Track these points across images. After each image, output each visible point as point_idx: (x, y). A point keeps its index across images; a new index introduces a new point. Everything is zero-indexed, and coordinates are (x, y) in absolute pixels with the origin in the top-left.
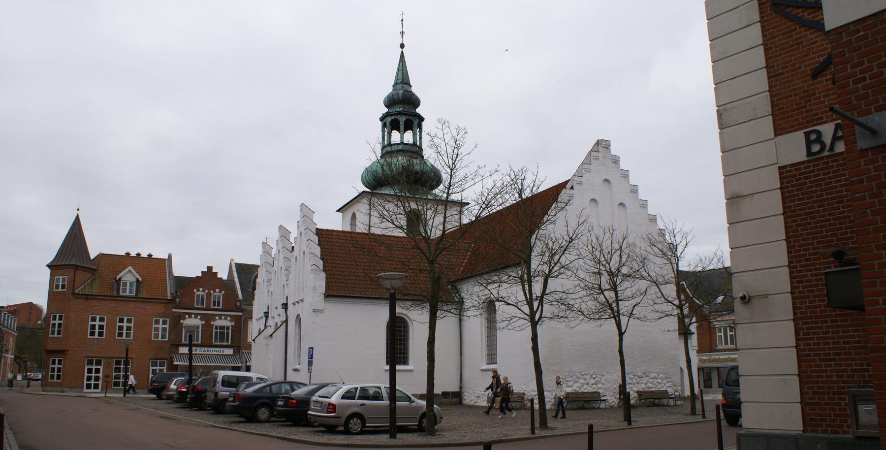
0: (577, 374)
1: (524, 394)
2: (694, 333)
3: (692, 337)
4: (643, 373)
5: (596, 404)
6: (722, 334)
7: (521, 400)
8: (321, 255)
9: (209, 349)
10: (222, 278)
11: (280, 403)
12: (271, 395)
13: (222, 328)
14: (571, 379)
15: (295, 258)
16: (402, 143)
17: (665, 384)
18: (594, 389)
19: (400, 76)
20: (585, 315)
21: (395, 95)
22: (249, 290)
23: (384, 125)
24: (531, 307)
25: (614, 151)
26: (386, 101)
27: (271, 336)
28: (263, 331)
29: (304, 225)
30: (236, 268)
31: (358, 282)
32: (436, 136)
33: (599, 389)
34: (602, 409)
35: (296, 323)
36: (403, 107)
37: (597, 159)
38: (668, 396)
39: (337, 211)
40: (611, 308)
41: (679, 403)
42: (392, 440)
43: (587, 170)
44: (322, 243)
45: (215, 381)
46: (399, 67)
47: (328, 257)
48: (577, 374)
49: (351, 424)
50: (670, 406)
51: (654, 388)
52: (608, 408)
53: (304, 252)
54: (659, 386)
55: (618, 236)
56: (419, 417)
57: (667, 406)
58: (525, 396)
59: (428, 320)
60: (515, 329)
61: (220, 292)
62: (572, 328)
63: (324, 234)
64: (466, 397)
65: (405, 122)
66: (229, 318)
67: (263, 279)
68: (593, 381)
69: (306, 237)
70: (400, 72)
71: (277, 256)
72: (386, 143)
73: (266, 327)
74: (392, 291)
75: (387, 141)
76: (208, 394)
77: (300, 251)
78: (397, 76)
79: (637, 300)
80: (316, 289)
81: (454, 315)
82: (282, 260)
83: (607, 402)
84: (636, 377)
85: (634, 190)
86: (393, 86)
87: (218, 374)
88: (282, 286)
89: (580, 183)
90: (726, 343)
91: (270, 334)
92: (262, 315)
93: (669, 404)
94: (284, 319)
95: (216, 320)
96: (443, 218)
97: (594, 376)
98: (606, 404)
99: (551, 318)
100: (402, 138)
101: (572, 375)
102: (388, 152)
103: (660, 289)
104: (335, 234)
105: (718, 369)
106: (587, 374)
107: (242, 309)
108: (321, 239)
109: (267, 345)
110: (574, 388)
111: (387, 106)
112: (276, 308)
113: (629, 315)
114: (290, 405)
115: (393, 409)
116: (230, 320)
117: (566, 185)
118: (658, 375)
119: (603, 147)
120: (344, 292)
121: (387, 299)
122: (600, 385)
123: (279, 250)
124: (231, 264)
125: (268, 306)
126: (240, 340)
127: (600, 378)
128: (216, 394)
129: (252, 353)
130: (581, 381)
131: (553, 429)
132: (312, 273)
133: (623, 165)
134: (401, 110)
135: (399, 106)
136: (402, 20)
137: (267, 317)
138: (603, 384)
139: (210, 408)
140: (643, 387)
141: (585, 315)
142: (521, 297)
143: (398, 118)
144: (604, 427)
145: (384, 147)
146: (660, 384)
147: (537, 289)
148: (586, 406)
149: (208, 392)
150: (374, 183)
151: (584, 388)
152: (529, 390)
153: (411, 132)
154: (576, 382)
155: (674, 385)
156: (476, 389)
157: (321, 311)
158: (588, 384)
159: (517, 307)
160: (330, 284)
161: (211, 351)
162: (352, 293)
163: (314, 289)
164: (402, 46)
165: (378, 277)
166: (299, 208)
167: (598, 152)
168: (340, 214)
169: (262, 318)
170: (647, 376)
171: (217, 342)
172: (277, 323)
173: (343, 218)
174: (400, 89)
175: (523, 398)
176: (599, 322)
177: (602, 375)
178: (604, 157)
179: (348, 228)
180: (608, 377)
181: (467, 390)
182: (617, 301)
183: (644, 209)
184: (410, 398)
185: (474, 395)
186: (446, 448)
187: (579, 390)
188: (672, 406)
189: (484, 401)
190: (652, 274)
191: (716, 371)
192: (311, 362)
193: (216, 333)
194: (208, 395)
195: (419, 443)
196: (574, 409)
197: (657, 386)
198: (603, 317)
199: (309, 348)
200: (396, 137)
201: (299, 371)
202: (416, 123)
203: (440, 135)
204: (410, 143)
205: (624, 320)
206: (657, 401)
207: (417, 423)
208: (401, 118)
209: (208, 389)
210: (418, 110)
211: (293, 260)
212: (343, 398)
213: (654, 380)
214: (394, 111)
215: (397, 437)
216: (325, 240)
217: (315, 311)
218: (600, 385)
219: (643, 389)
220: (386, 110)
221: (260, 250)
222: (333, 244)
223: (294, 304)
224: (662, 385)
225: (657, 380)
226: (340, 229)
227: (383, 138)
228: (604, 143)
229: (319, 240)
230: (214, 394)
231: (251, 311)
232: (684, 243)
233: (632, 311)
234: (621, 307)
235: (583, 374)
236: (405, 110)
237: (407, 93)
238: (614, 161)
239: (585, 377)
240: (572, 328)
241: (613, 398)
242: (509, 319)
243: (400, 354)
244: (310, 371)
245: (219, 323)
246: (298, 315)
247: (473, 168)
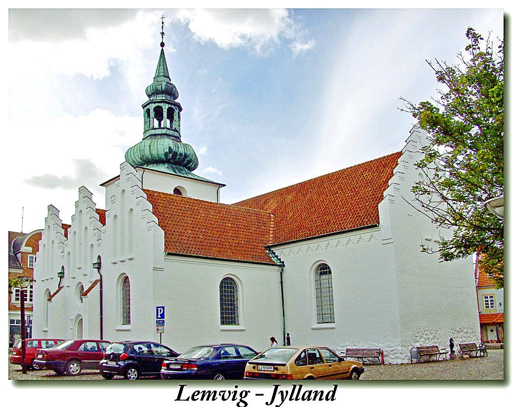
84: (456, 332)
111: (149, 96)
134: (163, 98)
138: (438, 339)
145: (145, 132)
158: (428, 339)
202: (177, 111)
217: (155, 269)
220: (147, 99)
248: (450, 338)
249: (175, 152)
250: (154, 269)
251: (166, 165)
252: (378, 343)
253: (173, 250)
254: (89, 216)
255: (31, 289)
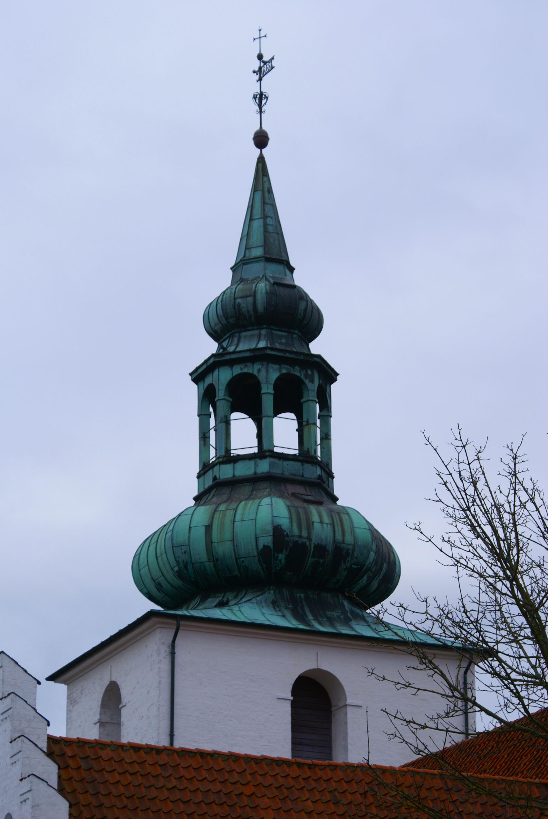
19: (257, 237)
36: (270, 337)
46: (251, 208)
65: (277, 385)
69: (18, 766)
70: (257, 224)
72: (213, 453)
78: (246, 236)
86: (234, 269)
111: (215, 335)
134: (262, 344)
135: (256, 332)
143: (255, 373)
150: (177, 582)
153: (292, 416)
173: (71, 701)
174: (257, 279)
202: (312, 387)
208: (263, 371)
227: (204, 437)
236: (278, 346)
249: (296, 543)
251: (270, 595)
253: (294, 269)
254: (17, 771)
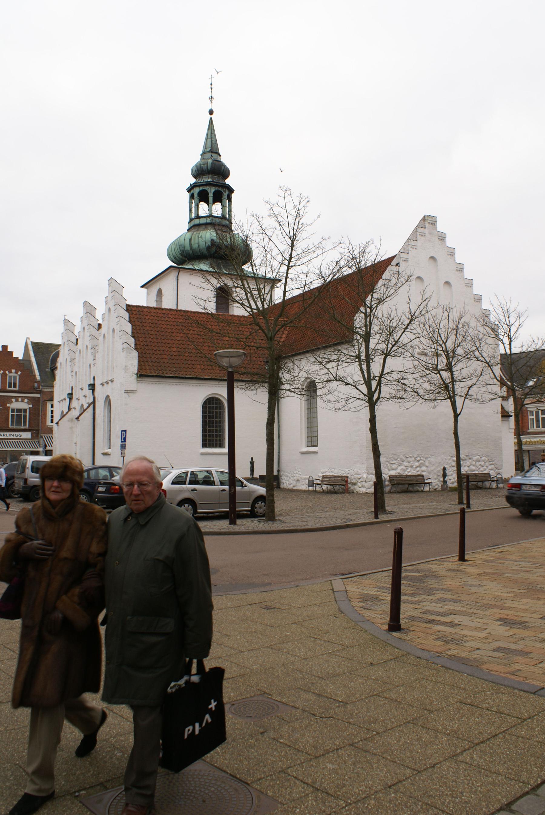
0: (401, 456)
1: (347, 477)
2: (511, 416)
3: (509, 420)
4: (467, 456)
5: (420, 487)
6: (534, 417)
7: (345, 484)
8: (132, 333)
9: (6, 433)
10: (18, 358)
11: (101, 489)
12: (90, 481)
13: (19, 410)
14: (395, 462)
15: (102, 335)
16: (210, 216)
17: (487, 467)
18: (418, 471)
19: (209, 145)
20: (420, 396)
21: (204, 164)
22: (47, 370)
23: (192, 197)
24: (369, 387)
25: (441, 227)
26: (194, 170)
27: (78, 418)
28: (67, 413)
29: (113, 301)
30: (33, 347)
31: (171, 361)
32: (277, 203)
33: (423, 471)
34: (426, 492)
35: (104, 404)
36: (212, 178)
37: (423, 235)
38: (491, 478)
39: (142, 287)
40: (446, 387)
41: (501, 485)
42: (233, 527)
43: (413, 247)
44: (133, 320)
45: (24, 468)
46: (207, 135)
47: (139, 335)
48: (401, 456)
49: (256, 508)
50: (492, 489)
51: (477, 470)
52: (432, 491)
53: (114, 330)
54: (482, 469)
55: (455, 315)
56: (251, 502)
57: (489, 488)
58: (349, 480)
59: (266, 400)
60: (351, 410)
61: (16, 373)
62: (407, 409)
63: (135, 311)
64: (284, 481)
66: (26, 400)
67: (65, 359)
68: (417, 464)
69: (116, 313)
70: (209, 140)
71: (82, 334)
73: (69, 409)
74: (230, 370)
75: (195, 214)
76: (16, 481)
77: (109, 328)
78: (206, 144)
79: (474, 381)
80: (128, 369)
81: (296, 395)
82: (87, 338)
83: (432, 485)
85: (460, 269)
86: (201, 155)
87: (26, 460)
88: (89, 365)
89: (406, 260)
90: (538, 426)
91: (76, 417)
92: (65, 396)
93: (491, 487)
94: (91, 400)
95: (12, 402)
96: (283, 293)
97: (418, 459)
98: (430, 487)
99: (389, 399)
100: (210, 210)
101: (396, 458)
102: (195, 226)
103: (492, 371)
104: (145, 310)
105: (529, 451)
106: (411, 457)
107: (40, 391)
108: (131, 316)
109: (71, 428)
110: (399, 471)
111: (195, 177)
112: (82, 389)
113: (465, 396)
114: (113, 491)
115: (233, 495)
116: (27, 403)
117: (391, 261)
118: (481, 458)
119: (429, 223)
120: (157, 372)
121: (224, 380)
122: (424, 468)
123: (84, 328)
124: (26, 342)
125: (72, 387)
126: (38, 423)
127: (424, 461)
128: (26, 480)
129: (53, 437)
130: (406, 464)
131: (392, 513)
132: (123, 351)
133: (449, 242)
134: (209, 180)
136: (211, 84)
137: (71, 399)
138: (427, 467)
139: (17, 496)
140: (466, 470)
141: (420, 396)
142: (358, 377)
144: (443, 511)
145: (191, 220)
146: (483, 466)
147: (376, 369)
148: (411, 489)
149: (15, 479)
150: (181, 257)
151: (408, 470)
152: (353, 474)
153: (220, 204)
154: (400, 464)
155: (496, 468)
156: (295, 472)
157: (133, 392)
158: (412, 467)
159: (355, 386)
160: (142, 363)
161: (8, 435)
162: (165, 372)
163: (126, 368)
164: (211, 112)
165: (215, 355)
166: (107, 283)
167: (425, 228)
168: (144, 290)
169: (65, 399)
170: (470, 459)
171: (13, 425)
172: (82, 405)
173: (148, 294)
174: (208, 159)
175: (347, 481)
176: (434, 404)
177: (427, 458)
178: (430, 233)
179: (153, 304)
180: (432, 459)
181: (284, 473)
182: (453, 381)
183: (469, 289)
184: (242, 483)
185: (293, 478)
186: (292, 534)
187: (403, 472)
188: (494, 489)
189: (303, 485)
190: (484, 354)
191: (527, 454)
192: (124, 445)
193: (13, 416)
194: (15, 481)
195: (264, 529)
196: (398, 492)
197: (479, 469)
198: (439, 398)
199: (122, 431)
200: (204, 210)
201: (110, 455)
202: (225, 194)
203: (282, 204)
204: (219, 216)
205: (459, 401)
206: (480, 484)
207: (250, 509)
209: (16, 475)
210: (227, 181)
211: (101, 338)
212: (173, 483)
213: (477, 463)
214: (202, 181)
215: (237, 523)
216: (135, 316)
217: (127, 392)
218: (424, 468)
219: (466, 472)
220: (193, 180)
221: (61, 328)
222: (144, 321)
223: (102, 385)
224: (485, 467)
225: (480, 463)
226: (145, 305)
227: (191, 210)
228: (430, 219)
229: (129, 317)
230: (23, 480)
231: (52, 393)
232: (517, 324)
233: (468, 392)
234: (456, 387)
235: (408, 456)
236: (214, 181)
237: (216, 162)
238: (440, 238)
239: (410, 459)
240: (407, 409)
241: (437, 481)
242: (346, 399)
243: (216, 436)
244: (123, 455)
245: (15, 405)
246: (108, 397)
247: (316, 240)
248: (442, 468)
250: (126, 392)
252: (349, 469)
255: (52, 409)
